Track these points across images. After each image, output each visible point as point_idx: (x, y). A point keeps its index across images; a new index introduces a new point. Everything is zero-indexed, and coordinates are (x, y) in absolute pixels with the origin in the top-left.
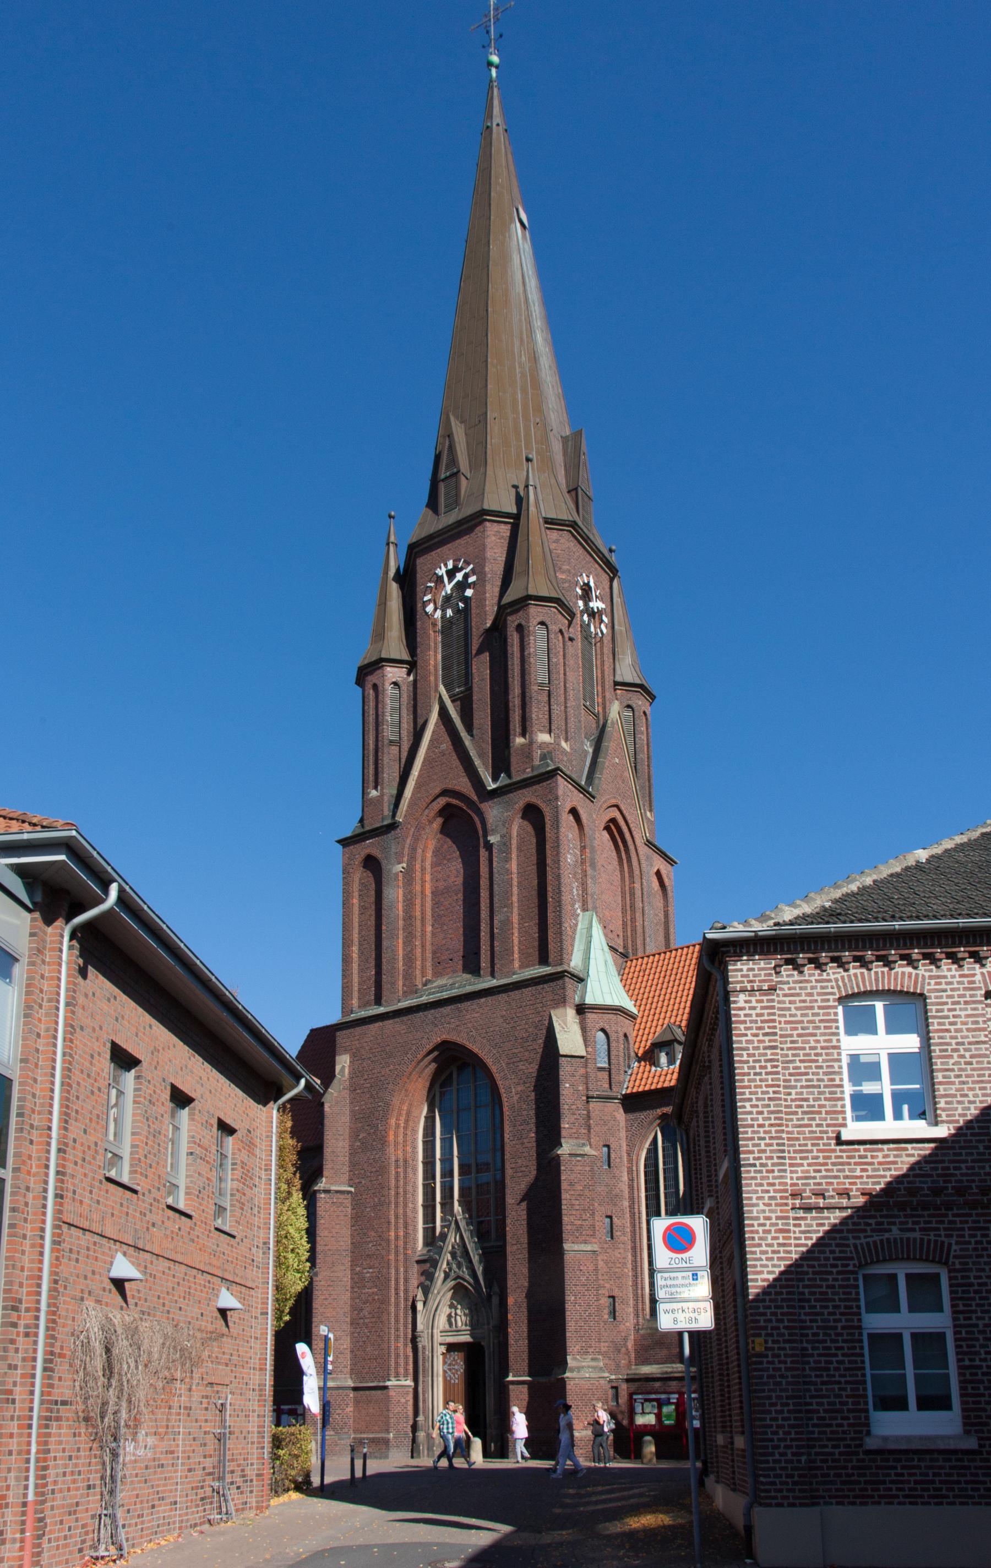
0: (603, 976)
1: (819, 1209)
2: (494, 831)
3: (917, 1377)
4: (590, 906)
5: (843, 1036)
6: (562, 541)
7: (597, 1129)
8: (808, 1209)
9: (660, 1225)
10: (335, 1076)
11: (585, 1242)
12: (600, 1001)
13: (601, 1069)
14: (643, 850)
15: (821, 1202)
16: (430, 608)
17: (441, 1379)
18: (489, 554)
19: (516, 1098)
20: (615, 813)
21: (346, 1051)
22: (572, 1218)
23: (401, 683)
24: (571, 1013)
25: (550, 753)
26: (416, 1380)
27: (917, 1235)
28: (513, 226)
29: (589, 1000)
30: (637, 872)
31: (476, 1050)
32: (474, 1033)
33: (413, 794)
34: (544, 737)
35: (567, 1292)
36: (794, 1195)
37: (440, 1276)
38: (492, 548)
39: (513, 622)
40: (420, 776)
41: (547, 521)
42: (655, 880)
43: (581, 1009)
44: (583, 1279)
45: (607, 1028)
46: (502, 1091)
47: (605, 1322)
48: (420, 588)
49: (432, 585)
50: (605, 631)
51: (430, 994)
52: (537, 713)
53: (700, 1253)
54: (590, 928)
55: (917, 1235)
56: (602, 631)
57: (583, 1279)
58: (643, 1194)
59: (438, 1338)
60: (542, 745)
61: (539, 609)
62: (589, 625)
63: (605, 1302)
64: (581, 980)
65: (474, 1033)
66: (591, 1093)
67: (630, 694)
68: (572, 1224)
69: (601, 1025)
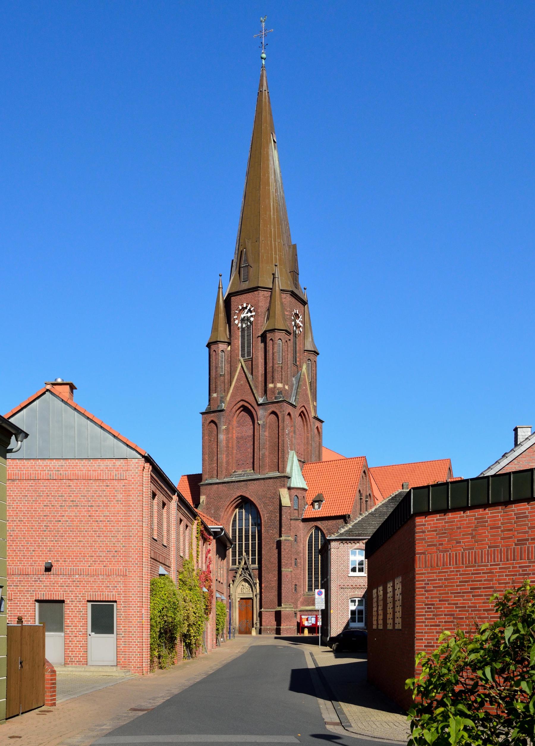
0: (297, 476)
1: (344, 588)
2: (261, 420)
3: (358, 617)
4: (293, 449)
5: (350, 555)
6: (287, 298)
7: (293, 530)
8: (342, 588)
9: (317, 591)
10: (199, 503)
11: (288, 568)
12: (296, 486)
13: (295, 509)
14: (312, 420)
15: (344, 587)
16: (236, 322)
17: (238, 609)
18: (260, 304)
19: (266, 518)
20: (303, 409)
21: (204, 495)
22: (285, 560)
23: (224, 351)
24: (286, 490)
25: (281, 391)
26: (230, 610)
27: (360, 593)
28: (270, 145)
29: (292, 486)
30: (308, 420)
31: (252, 500)
32: (252, 494)
33: (230, 399)
34: (279, 385)
35: (282, 584)
36: (340, 586)
37: (238, 575)
38: (261, 302)
39: (269, 337)
40: (232, 392)
41: (282, 290)
42: (316, 430)
43: (289, 488)
44: (287, 580)
45: (298, 495)
46: (261, 515)
47: (293, 593)
48: (232, 312)
49: (238, 312)
50: (301, 330)
51: (235, 477)
52: (277, 376)
53: (323, 596)
54: (293, 457)
55: (360, 593)
56: (300, 331)
57: (287, 580)
58: (307, 552)
59: (237, 596)
60: (278, 389)
61: (279, 334)
62: (296, 331)
63: (294, 586)
64: (289, 478)
65: (252, 494)
66: (291, 518)
67: (310, 355)
68: (285, 562)
69: (296, 494)
